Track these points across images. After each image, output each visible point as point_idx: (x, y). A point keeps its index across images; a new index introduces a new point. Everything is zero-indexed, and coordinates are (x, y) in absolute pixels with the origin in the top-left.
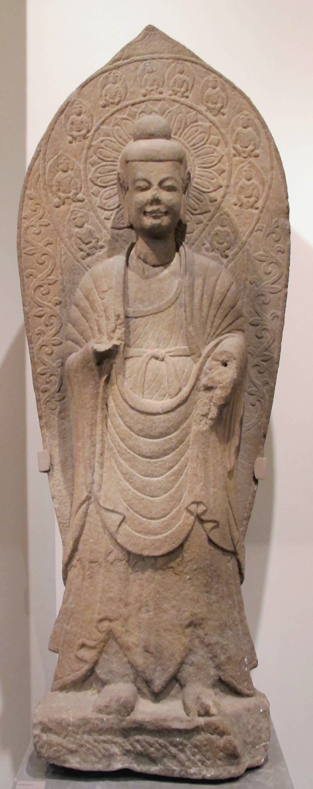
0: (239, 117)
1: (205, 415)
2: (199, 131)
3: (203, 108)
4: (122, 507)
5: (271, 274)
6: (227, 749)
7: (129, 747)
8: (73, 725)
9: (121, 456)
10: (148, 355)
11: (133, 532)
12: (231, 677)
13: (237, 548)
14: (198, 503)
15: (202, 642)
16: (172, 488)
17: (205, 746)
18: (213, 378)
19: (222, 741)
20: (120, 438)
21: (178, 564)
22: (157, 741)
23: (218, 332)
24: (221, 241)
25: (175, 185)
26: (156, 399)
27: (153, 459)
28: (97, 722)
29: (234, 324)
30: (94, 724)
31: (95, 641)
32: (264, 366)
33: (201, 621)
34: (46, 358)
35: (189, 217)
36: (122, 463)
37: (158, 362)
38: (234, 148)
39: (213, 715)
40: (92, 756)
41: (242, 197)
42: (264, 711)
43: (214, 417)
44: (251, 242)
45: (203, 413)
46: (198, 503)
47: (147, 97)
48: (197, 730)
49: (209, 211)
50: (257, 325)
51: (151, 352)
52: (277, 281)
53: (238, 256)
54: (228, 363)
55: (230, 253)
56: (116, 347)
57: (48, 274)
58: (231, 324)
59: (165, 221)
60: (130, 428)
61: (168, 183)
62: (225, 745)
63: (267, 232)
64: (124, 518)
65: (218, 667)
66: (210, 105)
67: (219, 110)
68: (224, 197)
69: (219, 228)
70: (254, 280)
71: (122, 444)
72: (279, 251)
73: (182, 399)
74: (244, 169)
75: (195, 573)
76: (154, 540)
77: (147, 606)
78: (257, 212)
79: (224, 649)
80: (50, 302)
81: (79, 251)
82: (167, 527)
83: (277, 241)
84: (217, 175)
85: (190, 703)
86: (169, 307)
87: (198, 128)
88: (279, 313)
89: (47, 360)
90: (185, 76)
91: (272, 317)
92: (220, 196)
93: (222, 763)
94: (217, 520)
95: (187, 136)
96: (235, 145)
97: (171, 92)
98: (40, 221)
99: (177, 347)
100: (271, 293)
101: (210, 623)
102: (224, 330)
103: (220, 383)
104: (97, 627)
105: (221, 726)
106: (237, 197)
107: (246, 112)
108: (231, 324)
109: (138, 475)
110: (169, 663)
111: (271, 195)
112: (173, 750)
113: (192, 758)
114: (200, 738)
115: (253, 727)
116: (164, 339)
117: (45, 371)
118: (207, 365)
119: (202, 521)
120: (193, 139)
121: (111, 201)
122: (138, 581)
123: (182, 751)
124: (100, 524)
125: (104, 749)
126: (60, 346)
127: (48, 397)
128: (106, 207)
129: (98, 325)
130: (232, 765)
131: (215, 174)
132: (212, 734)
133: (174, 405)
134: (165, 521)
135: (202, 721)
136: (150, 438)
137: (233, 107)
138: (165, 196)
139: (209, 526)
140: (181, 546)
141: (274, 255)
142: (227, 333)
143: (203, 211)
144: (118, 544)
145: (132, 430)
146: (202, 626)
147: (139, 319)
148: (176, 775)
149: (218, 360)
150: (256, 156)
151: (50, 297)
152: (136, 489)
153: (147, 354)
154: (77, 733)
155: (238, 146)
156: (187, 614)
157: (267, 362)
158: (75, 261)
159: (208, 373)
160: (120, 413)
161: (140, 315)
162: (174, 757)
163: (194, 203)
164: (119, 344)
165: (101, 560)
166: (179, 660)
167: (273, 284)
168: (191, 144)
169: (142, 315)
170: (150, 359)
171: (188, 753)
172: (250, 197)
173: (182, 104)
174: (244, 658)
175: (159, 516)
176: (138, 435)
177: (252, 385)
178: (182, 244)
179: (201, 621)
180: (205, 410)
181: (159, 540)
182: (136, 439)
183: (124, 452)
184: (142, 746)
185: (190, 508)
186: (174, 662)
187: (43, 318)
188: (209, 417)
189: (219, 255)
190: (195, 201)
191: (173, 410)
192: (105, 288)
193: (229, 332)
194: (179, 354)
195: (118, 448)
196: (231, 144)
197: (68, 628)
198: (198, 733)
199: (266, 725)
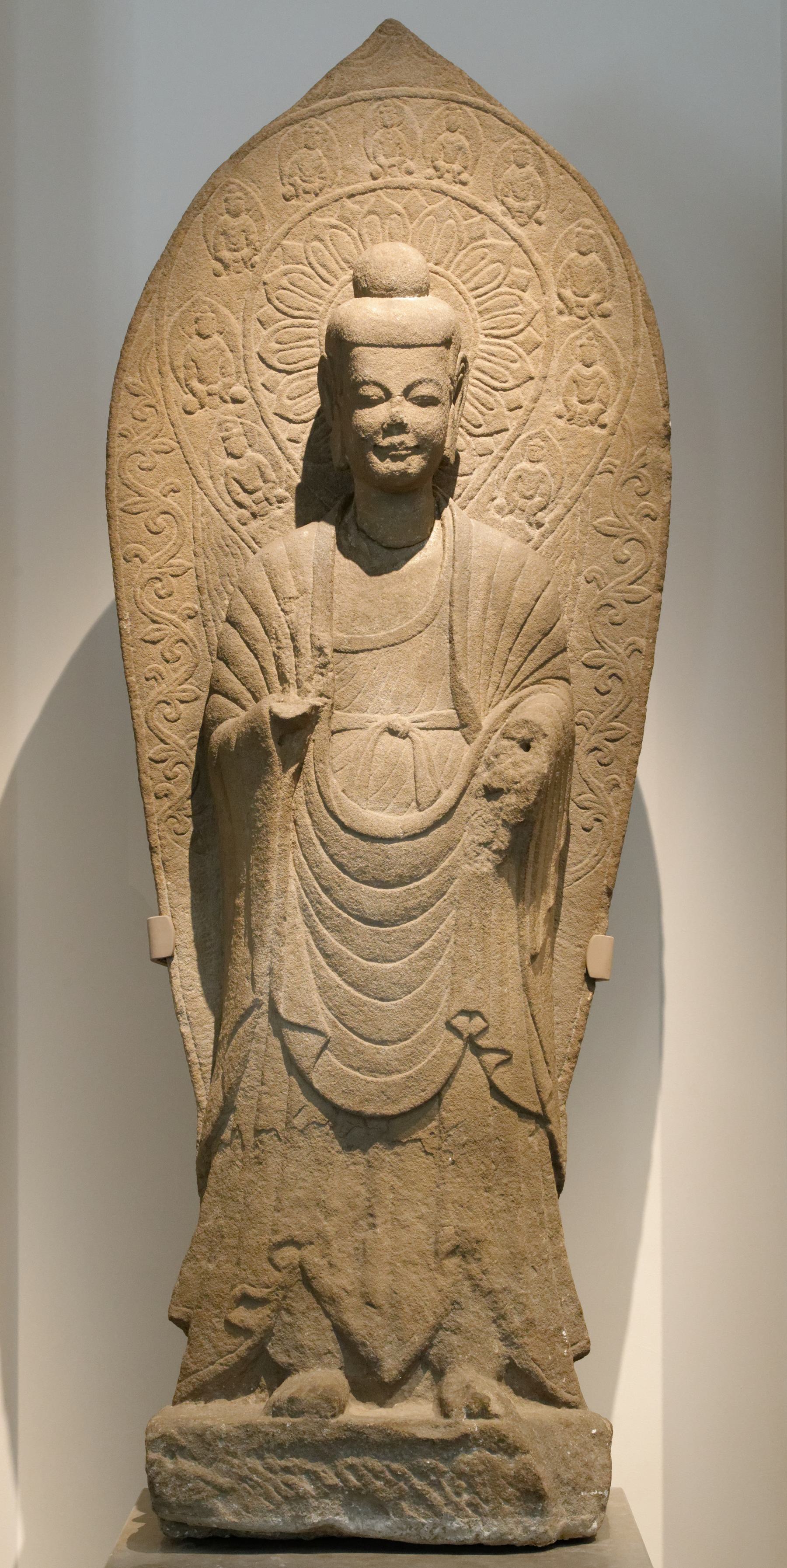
0: (571, 232)
1: (486, 845)
2: (488, 258)
3: (495, 208)
4: (324, 1020)
5: (629, 563)
6: (522, 1481)
7: (335, 1480)
8: (228, 1438)
9: (322, 921)
10: (378, 727)
11: (344, 1068)
12: (534, 1360)
13: (549, 1107)
14: (470, 1014)
15: (476, 1287)
16: (422, 983)
17: (480, 1473)
18: (501, 773)
19: (510, 1466)
20: (322, 886)
21: (432, 1133)
22: (388, 1467)
23: (516, 682)
24: (528, 493)
25: (435, 394)
26: (393, 811)
27: (386, 926)
28: (272, 1430)
29: (549, 665)
30: (267, 1434)
31: (268, 1287)
32: (610, 751)
33: (475, 1246)
34: (165, 729)
35: (465, 440)
36: (325, 935)
37: (396, 740)
38: (561, 297)
39: (496, 1416)
40: (262, 1499)
41: (574, 400)
42: (600, 1434)
43: (503, 848)
44: (590, 496)
45: (482, 839)
46: (470, 1014)
47: (380, 182)
48: (464, 1441)
49: (506, 430)
50: (599, 668)
51: (382, 719)
52: (640, 577)
53: (562, 523)
54: (532, 744)
55: (546, 517)
56: (316, 709)
57: (171, 554)
58: (541, 666)
59: (415, 464)
60: (340, 866)
61: (423, 390)
62: (518, 1472)
63: (624, 477)
64: (328, 1042)
65: (507, 1338)
66: (510, 201)
67: (530, 213)
68: (536, 400)
69: (525, 464)
70: (594, 574)
71: (325, 898)
72: (647, 516)
73: (442, 811)
74: (579, 342)
75: (465, 1150)
76: (385, 1083)
77: (372, 1215)
78: (604, 432)
79: (522, 1306)
80: (175, 612)
81: (236, 507)
82: (411, 1059)
83: (642, 495)
84: (524, 354)
85: (450, 1396)
86: (420, 632)
87: (486, 250)
88: (642, 643)
89: (169, 733)
90: (462, 137)
91: (628, 652)
92: (529, 399)
93: (512, 1509)
94: (509, 1048)
95: (463, 267)
96: (562, 290)
97: (431, 171)
98: (154, 441)
99: (433, 712)
100: (628, 602)
101: (493, 1250)
102: (527, 677)
103: (516, 783)
104: (270, 1260)
105: (511, 1435)
106: (564, 401)
107: (587, 221)
108: (541, 666)
109: (355, 957)
110: (412, 1326)
111: (633, 398)
112: (419, 1484)
113: (456, 1499)
114: (469, 1458)
115: (575, 1455)
116: (409, 696)
117: (164, 755)
118: (491, 746)
119: (478, 1051)
120: (475, 274)
121: (303, 403)
122: (352, 1167)
123: (438, 1486)
124: (281, 1055)
125: (287, 1484)
126: (196, 703)
127: (170, 808)
128: (291, 416)
129: (279, 666)
130: (532, 1513)
131: (520, 350)
132: (492, 1451)
133: (428, 823)
134: (406, 1047)
135: (474, 1425)
136: (379, 887)
137: (560, 208)
138: (410, 413)
139: (492, 1059)
140: (438, 1096)
141: (636, 523)
142: (533, 684)
143: (492, 430)
144: (316, 1092)
145: (345, 872)
146: (478, 1256)
147: (361, 655)
148: (426, 1537)
149: (513, 739)
150: (604, 316)
151: (173, 602)
152: (351, 984)
153: (375, 724)
154: (234, 1455)
155: (568, 293)
156: (449, 1231)
157: (617, 743)
158: (225, 527)
159: (493, 763)
160: (322, 837)
161: (362, 648)
162: (420, 1498)
163: (475, 411)
164: (321, 704)
165: (281, 1126)
166: (432, 1320)
167: (632, 583)
168: (472, 285)
169: (366, 647)
170: (381, 733)
171: (448, 1489)
172: (590, 401)
173: (455, 199)
174: (560, 1329)
175: (396, 1036)
176: (357, 880)
177: (586, 789)
178: (447, 502)
179: (475, 1246)
180: (486, 834)
181: (395, 1084)
182: (353, 889)
183: (327, 912)
184: (360, 1477)
185: (454, 1022)
186: (422, 1325)
187: (159, 646)
188: (494, 847)
189: (523, 521)
190: (476, 408)
191: (425, 832)
192: (294, 592)
193: (538, 682)
194: (439, 725)
195: (318, 906)
196: (553, 290)
197: (211, 1267)
198: (468, 1450)
199: (601, 1460)
